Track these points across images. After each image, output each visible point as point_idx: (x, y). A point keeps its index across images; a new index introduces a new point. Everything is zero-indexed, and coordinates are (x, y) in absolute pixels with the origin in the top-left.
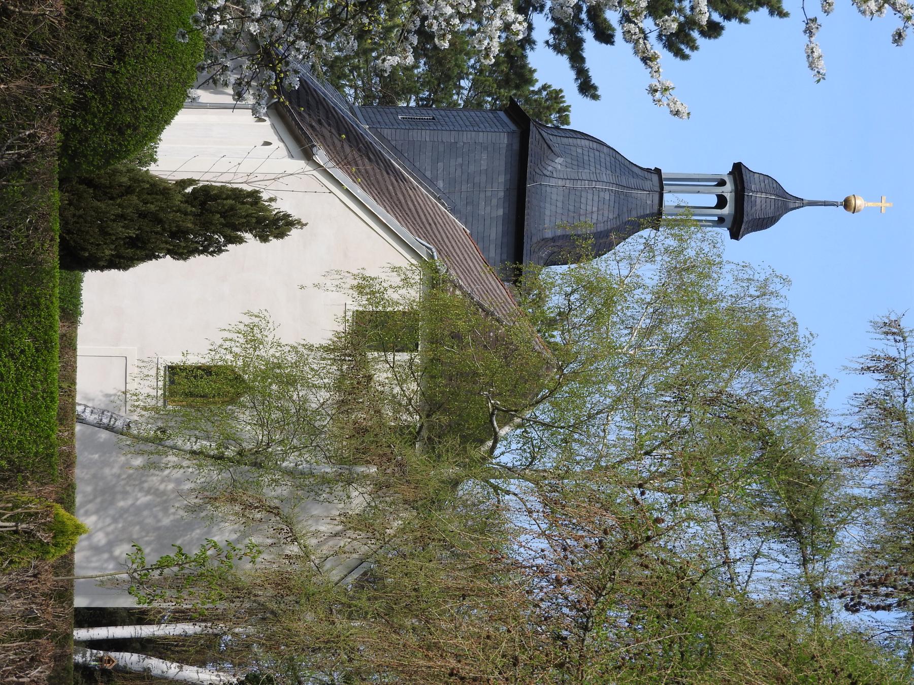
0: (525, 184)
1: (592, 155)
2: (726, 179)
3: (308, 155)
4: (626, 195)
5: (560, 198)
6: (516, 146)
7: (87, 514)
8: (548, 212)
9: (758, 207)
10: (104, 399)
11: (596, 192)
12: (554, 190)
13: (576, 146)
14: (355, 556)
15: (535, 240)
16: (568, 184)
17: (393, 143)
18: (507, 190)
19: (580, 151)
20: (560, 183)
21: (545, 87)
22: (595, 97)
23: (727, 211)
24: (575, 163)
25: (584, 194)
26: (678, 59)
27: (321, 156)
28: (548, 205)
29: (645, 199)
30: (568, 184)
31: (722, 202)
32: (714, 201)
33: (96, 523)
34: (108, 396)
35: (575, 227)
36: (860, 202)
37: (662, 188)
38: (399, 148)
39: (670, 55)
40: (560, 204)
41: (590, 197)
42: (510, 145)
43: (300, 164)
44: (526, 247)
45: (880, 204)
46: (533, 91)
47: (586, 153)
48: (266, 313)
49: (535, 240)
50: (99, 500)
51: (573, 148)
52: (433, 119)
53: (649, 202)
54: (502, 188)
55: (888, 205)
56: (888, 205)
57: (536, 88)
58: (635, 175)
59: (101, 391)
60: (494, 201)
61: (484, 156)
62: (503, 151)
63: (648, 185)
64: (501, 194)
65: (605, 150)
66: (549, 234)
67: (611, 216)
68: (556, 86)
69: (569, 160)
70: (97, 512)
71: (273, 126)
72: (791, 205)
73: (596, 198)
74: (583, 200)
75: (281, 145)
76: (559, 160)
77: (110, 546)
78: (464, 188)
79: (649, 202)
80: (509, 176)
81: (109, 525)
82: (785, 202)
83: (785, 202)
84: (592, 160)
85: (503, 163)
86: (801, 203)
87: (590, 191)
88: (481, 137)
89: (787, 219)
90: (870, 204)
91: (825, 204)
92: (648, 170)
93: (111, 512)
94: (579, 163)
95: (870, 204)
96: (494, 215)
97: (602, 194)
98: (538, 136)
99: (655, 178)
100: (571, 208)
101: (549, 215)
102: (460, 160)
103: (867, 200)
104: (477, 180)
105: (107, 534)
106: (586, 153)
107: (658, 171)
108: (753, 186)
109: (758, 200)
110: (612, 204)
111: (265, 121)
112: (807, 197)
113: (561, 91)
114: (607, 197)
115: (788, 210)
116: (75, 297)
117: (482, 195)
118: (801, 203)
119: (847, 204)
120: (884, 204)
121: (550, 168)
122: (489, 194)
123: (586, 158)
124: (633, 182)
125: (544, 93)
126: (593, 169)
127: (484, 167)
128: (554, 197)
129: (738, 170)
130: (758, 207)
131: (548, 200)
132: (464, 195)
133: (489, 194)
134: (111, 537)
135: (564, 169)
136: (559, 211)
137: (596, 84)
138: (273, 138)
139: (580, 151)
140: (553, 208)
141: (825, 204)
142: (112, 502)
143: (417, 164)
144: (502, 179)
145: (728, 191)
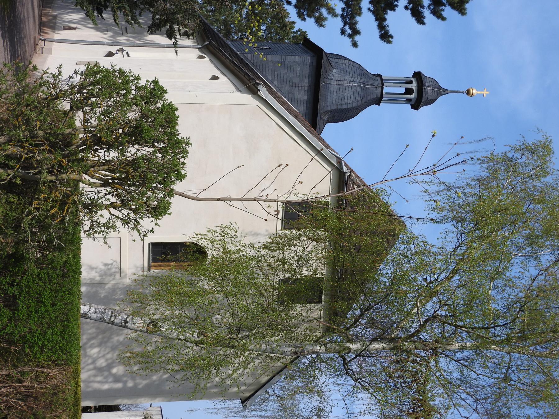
0: (319, 84)
1: (350, 68)
2: (413, 79)
3: (254, 91)
4: (366, 88)
5: (335, 90)
6: (314, 64)
7: (92, 347)
8: (329, 98)
9: (429, 94)
10: (103, 267)
11: (353, 87)
12: (332, 86)
13: (343, 63)
14: (279, 364)
15: (322, 112)
16: (340, 83)
17: (252, 61)
18: (309, 86)
19: (344, 66)
20: (336, 82)
21: (299, 30)
22: (389, 42)
23: (413, 96)
24: (342, 72)
25: (347, 88)
26: (440, 20)
27: (263, 92)
28: (329, 94)
29: (375, 92)
30: (340, 83)
31: (409, 91)
32: (403, 90)
33: (99, 352)
34: (106, 265)
35: (341, 104)
36: (475, 92)
37: (383, 85)
38: (255, 64)
39: (434, 18)
40: (335, 93)
41: (350, 89)
42: (311, 63)
43: (248, 98)
44: (319, 115)
45: (483, 92)
46: (294, 32)
47: (347, 67)
48: (235, 226)
49: (322, 112)
50: (100, 337)
51: (341, 64)
52: (269, 48)
53: (376, 92)
54: (307, 85)
55: (487, 93)
56: (487, 93)
57: (295, 30)
58: (370, 78)
59: (102, 262)
60: (303, 92)
61: (298, 69)
62: (308, 66)
63: (376, 83)
64: (306, 88)
65: (347, 61)
66: (329, 109)
67: (359, 99)
68: (304, 30)
69: (339, 71)
70: (100, 345)
71: (210, 60)
72: (443, 93)
73: (353, 90)
74: (347, 91)
75: (225, 78)
76: (335, 71)
77: (110, 366)
78: (288, 85)
79: (376, 92)
80: (310, 79)
81: (108, 353)
82: (440, 91)
83: (440, 91)
84: (351, 70)
85: (308, 72)
86: (447, 92)
87: (350, 87)
88: (297, 59)
89: (440, 99)
90: (479, 92)
91: (458, 92)
92: (374, 75)
93: (109, 344)
94: (344, 72)
95: (479, 92)
96: (302, 99)
97: (355, 88)
98: (326, 59)
99: (379, 79)
100: (340, 95)
101: (331, 99)
102: (286, 71)
103: (478, 90)
104: (294, 81)
105: (107, 360)
106: (347, 67)
107: (380, 76)
108: (427, 83)
109: (429, 90)
110: (360, 93)
111: (205, 58)
112: (450, 89)
113: (306, 32)
114: (358, 89)
115: (441, 95)
116: (64, 350)
117: (297, 89)
118: (447, 92)
119: (468, 92)
120: (485, 93)
121: (330, 75)
122: (300, 88)
123: (348, 69)
124: (370, 81)
125: (299, 33)
126: (351, 75)
127: (298, 74)
128: (332, 89)
129: (418, 75)
130: (429, 94)
131: (329, 91)
132: (287, 89)
133: (300, 88)
134: (110, 361)
135: (337, 75)
136: (335, 97)
137: (392, 35)
138: (217, 73)
139: (344, 66)
140: (332, 95)
141: (458, 92)
142: (109, 338)
143: (264, 73)
144: (307, 80)
145: (414, 86)
